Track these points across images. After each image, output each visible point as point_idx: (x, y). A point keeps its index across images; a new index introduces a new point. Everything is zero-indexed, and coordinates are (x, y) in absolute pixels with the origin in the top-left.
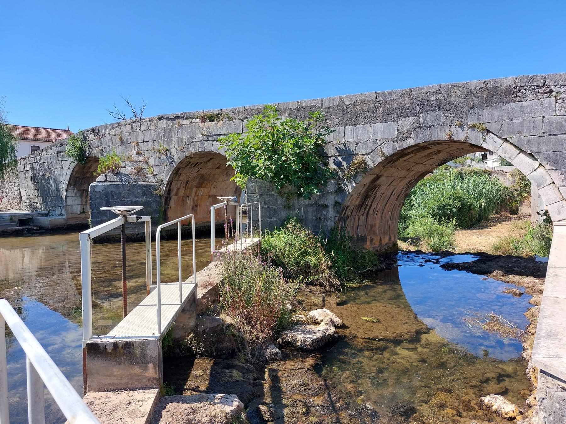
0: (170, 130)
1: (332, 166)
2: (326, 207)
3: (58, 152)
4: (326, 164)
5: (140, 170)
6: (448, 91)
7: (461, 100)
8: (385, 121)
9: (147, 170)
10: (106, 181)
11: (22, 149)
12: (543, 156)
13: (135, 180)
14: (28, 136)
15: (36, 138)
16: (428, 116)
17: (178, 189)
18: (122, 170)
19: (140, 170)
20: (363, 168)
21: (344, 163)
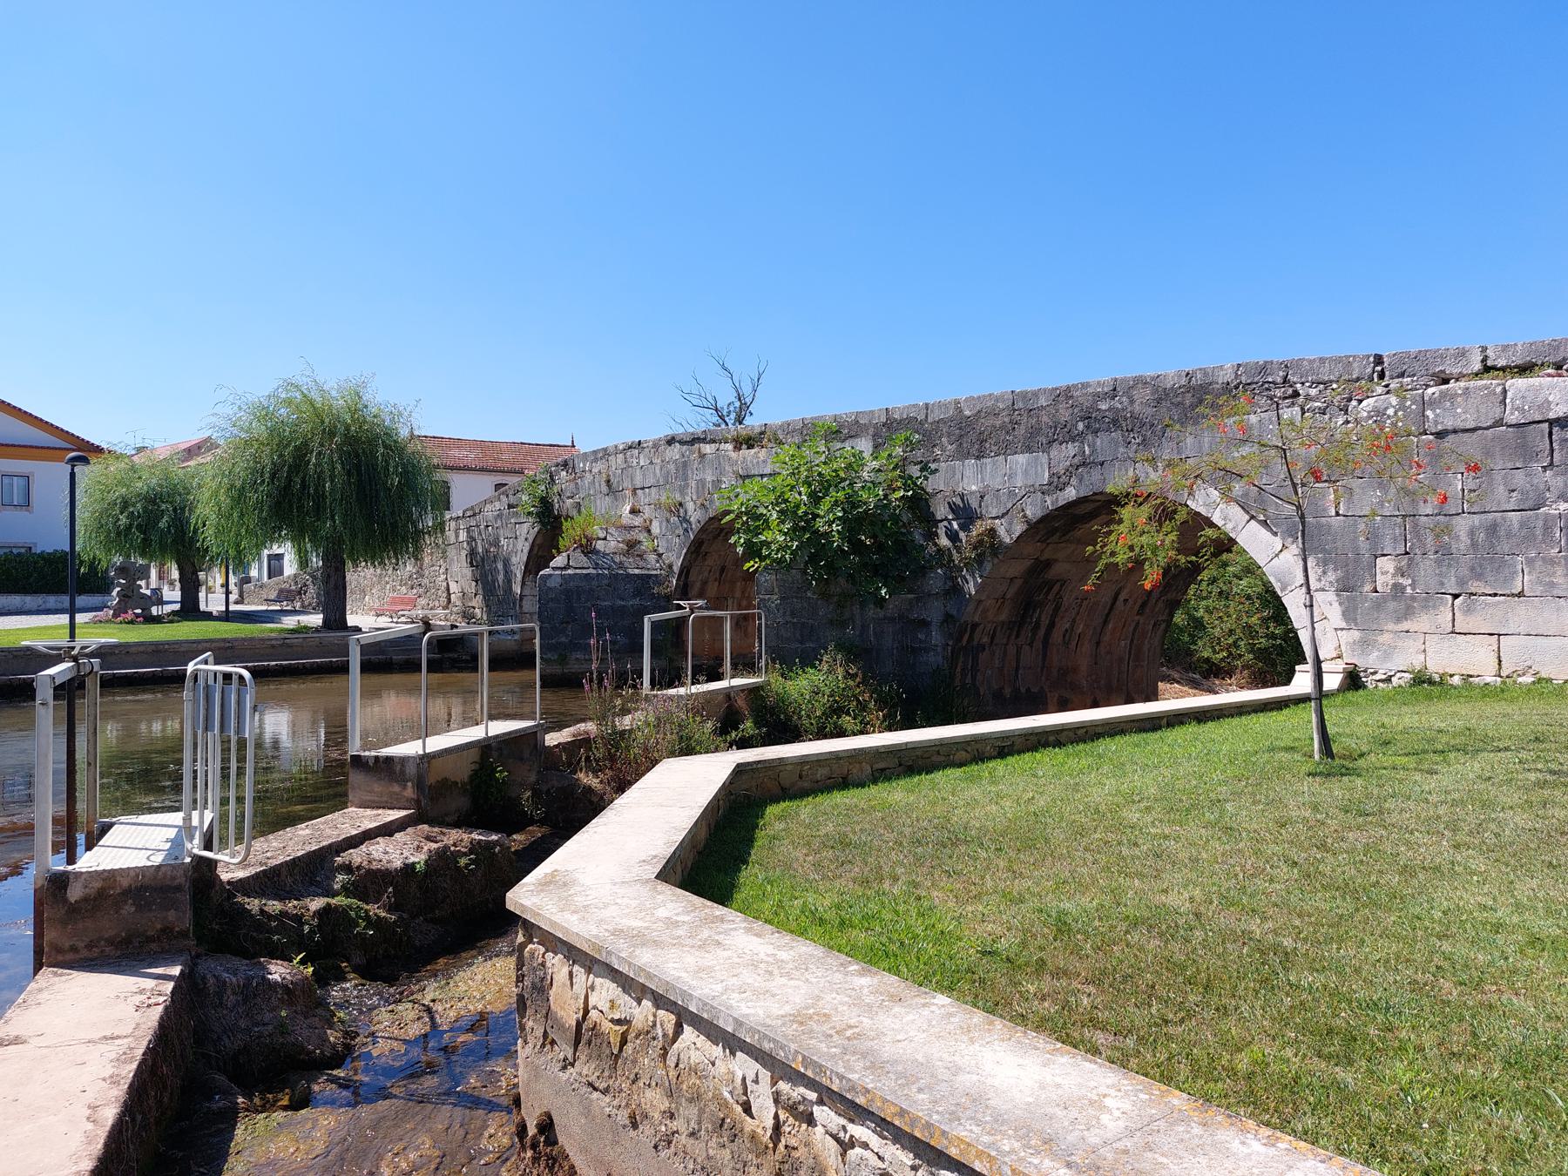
0: (685, 464)
1: (944, 541)
2: (924, 624)
3: (510, 506)
4: (931, 536)
5: (632, 545)
6: (1128, 392)
7: (1150, 411)
8: (1029, 450)
9: (646, 544)
10: (567, 567)
11: (466, 491)
12: (1284, 527)
13: (621, 565)
14: (490, 463)
15: (507, 466)
16: (1098, 442)
17: (705, 583)
18: (600, 545)
19: (632, 545)
20: (989, 546)
21: (962, 535)
